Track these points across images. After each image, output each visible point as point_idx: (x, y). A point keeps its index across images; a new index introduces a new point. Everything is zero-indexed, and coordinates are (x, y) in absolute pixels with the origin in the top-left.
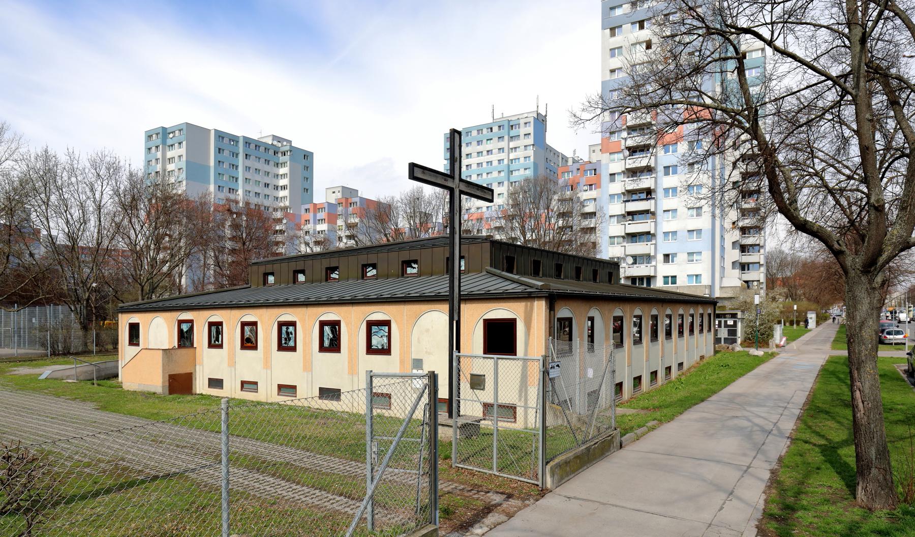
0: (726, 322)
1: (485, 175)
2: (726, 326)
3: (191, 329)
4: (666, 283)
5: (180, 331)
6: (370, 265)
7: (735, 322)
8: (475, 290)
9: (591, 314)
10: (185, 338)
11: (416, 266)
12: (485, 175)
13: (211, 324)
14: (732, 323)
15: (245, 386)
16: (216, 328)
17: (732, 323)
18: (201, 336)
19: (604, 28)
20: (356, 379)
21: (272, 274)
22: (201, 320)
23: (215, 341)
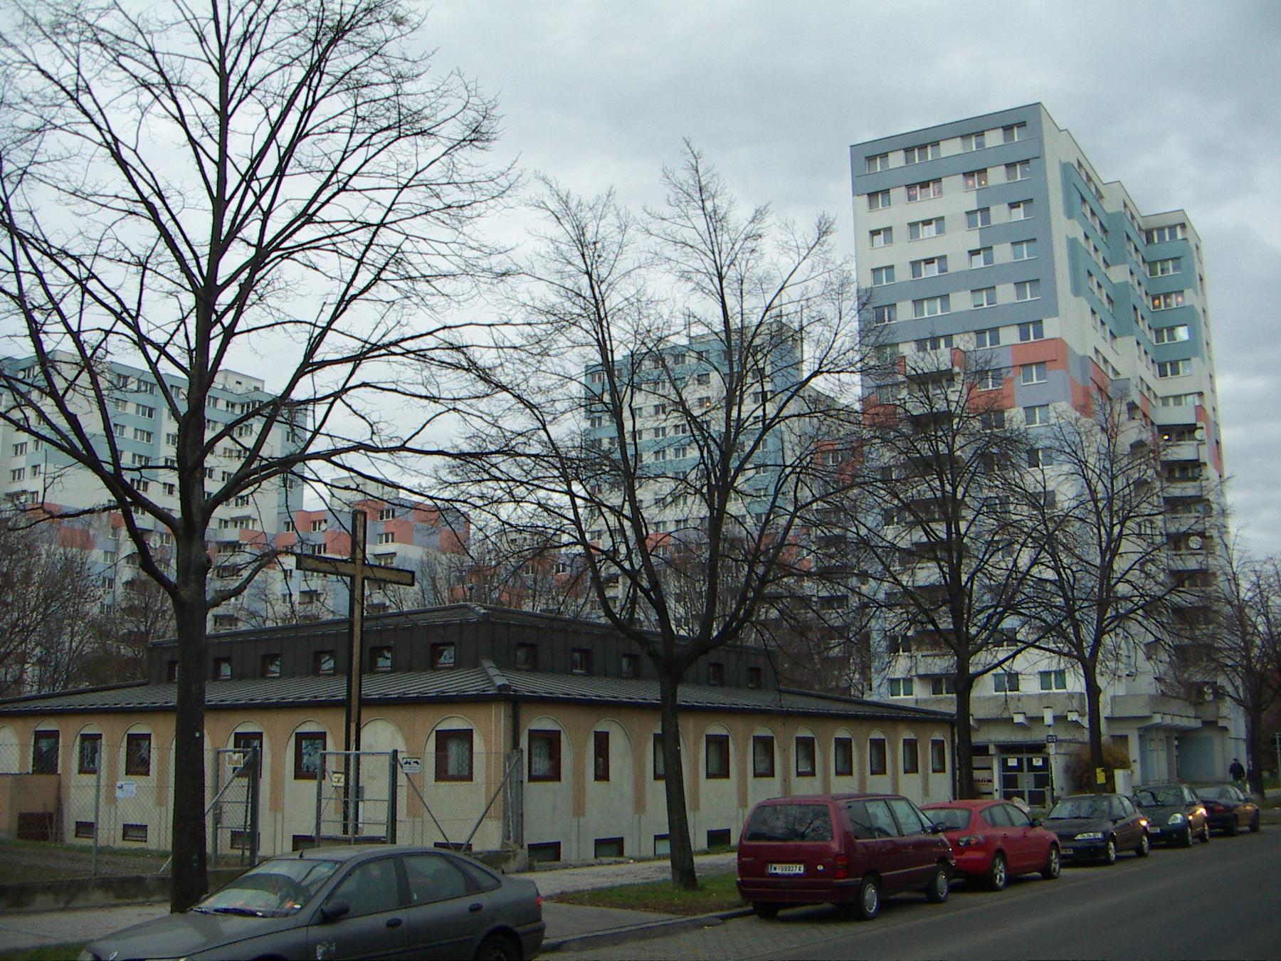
0: (1030, 761)
1: (670, 454)
2: (1032, 768)
3: (54, 749)
4: (1045, 685)
5: (37, 751)
6: (326, 652)
7: (1046, 761)
8: (692, 702)
9: (602, 727)
10: (45, 762)
11: (389, 655)
12: (670, 454)
13: (85, 738)
14: (1040, 763)
15: (131, 833)
16: (90, 742)
17: (1040, 763)
18: (69, 757)
19: (856, 193)
20: (279, 816)
21: (227, 660)
22: (70, 735)
23: (88, 765)
